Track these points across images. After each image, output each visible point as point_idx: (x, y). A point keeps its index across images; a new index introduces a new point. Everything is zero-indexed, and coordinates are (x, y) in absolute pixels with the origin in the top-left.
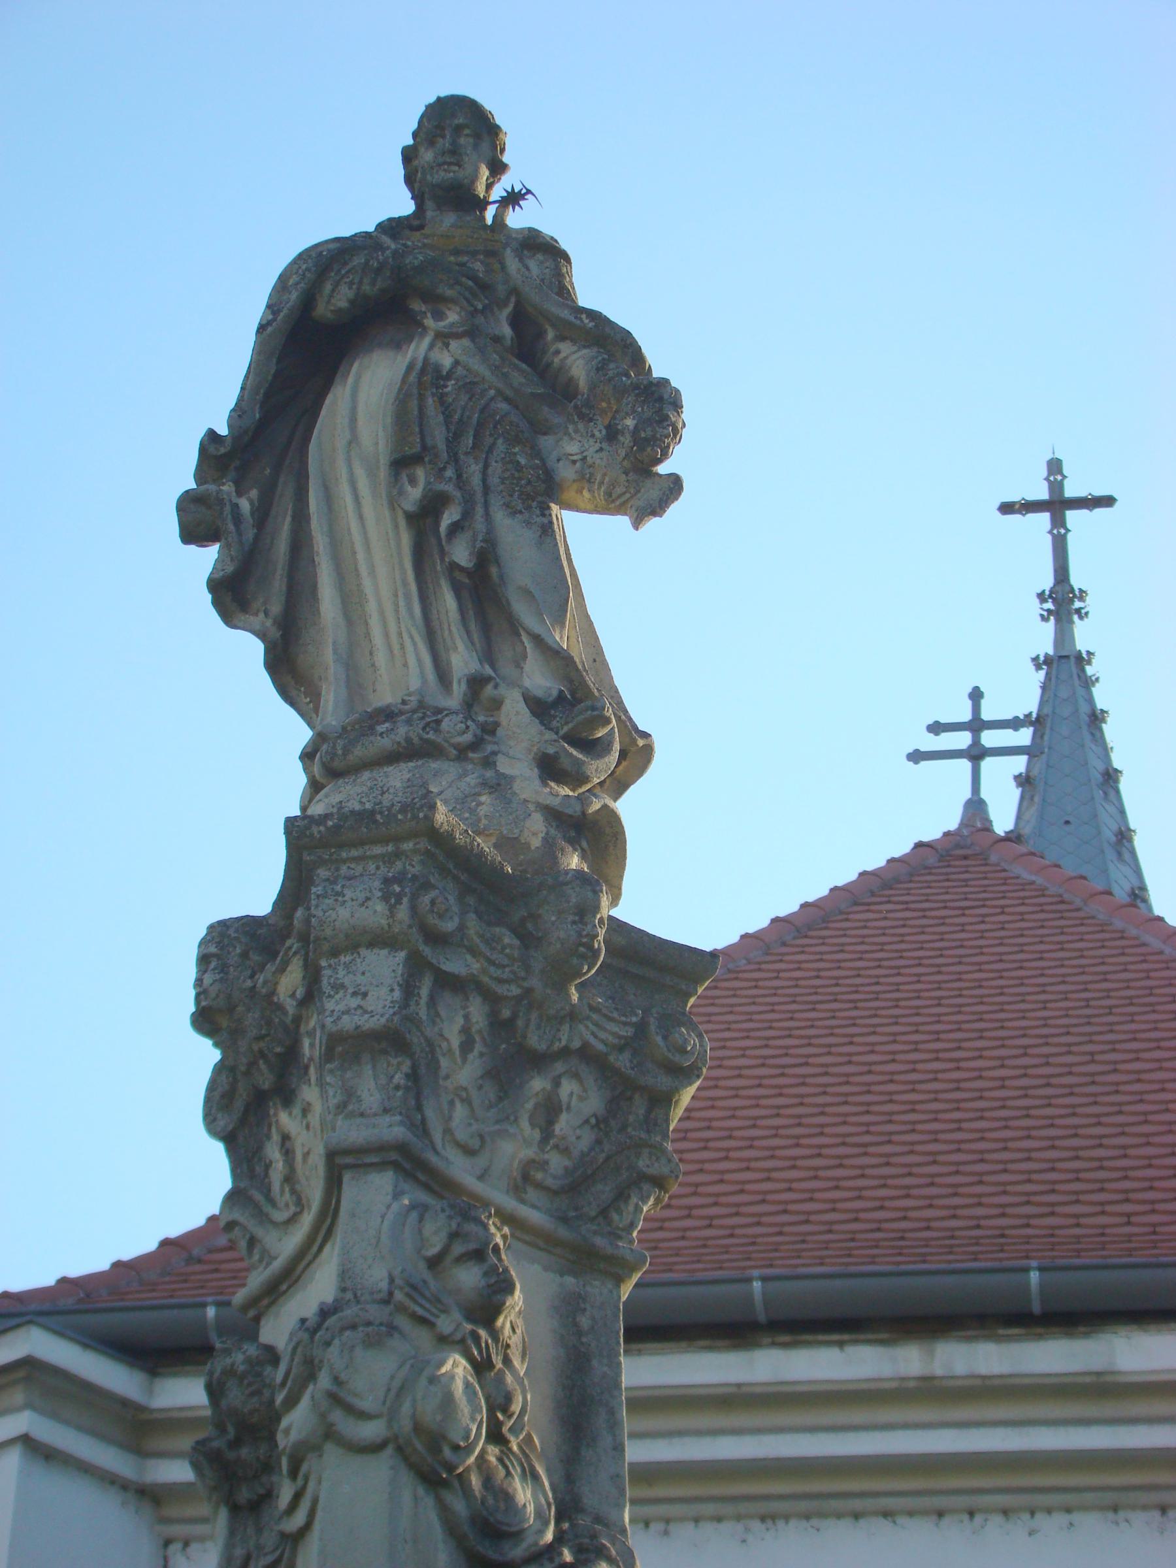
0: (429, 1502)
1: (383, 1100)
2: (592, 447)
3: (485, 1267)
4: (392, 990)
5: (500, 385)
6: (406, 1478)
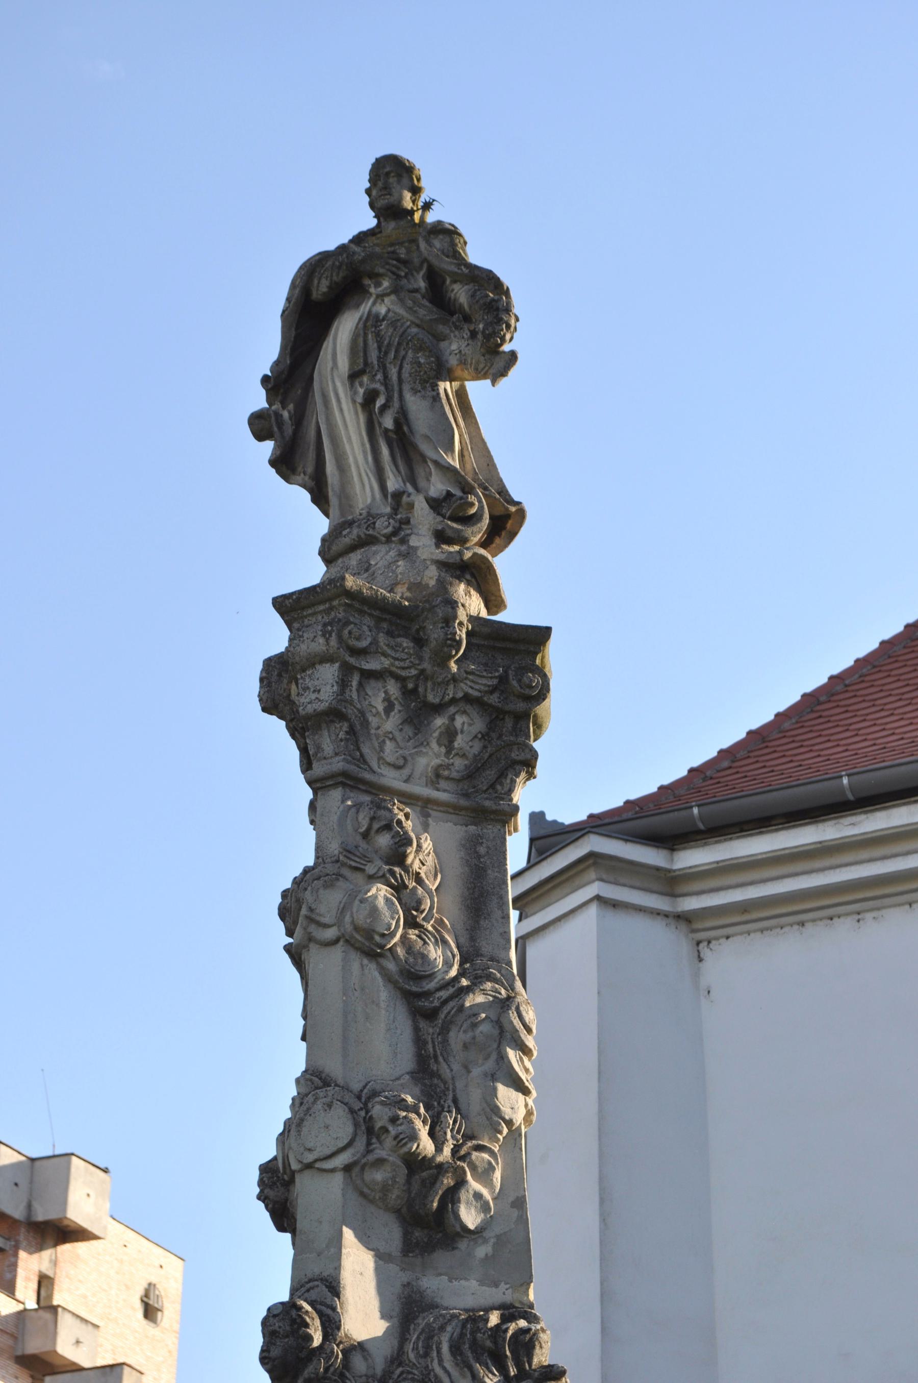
0: (373, 966)
1: (335, 748)
2: (463, 344)
3: (392, 833)
4: (333, 686)
5: (412, 318)
6: (354, 957)
